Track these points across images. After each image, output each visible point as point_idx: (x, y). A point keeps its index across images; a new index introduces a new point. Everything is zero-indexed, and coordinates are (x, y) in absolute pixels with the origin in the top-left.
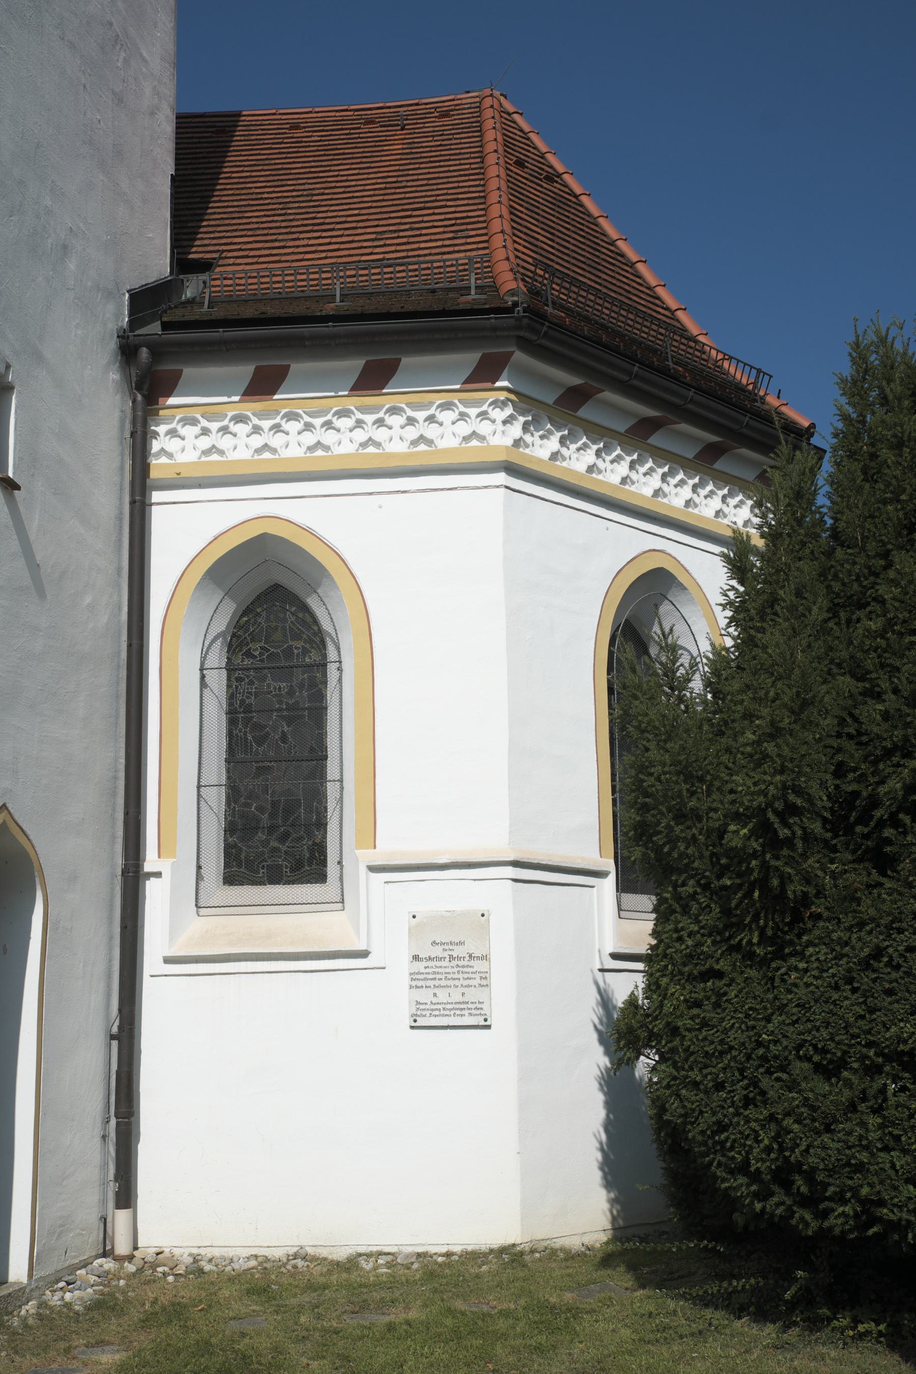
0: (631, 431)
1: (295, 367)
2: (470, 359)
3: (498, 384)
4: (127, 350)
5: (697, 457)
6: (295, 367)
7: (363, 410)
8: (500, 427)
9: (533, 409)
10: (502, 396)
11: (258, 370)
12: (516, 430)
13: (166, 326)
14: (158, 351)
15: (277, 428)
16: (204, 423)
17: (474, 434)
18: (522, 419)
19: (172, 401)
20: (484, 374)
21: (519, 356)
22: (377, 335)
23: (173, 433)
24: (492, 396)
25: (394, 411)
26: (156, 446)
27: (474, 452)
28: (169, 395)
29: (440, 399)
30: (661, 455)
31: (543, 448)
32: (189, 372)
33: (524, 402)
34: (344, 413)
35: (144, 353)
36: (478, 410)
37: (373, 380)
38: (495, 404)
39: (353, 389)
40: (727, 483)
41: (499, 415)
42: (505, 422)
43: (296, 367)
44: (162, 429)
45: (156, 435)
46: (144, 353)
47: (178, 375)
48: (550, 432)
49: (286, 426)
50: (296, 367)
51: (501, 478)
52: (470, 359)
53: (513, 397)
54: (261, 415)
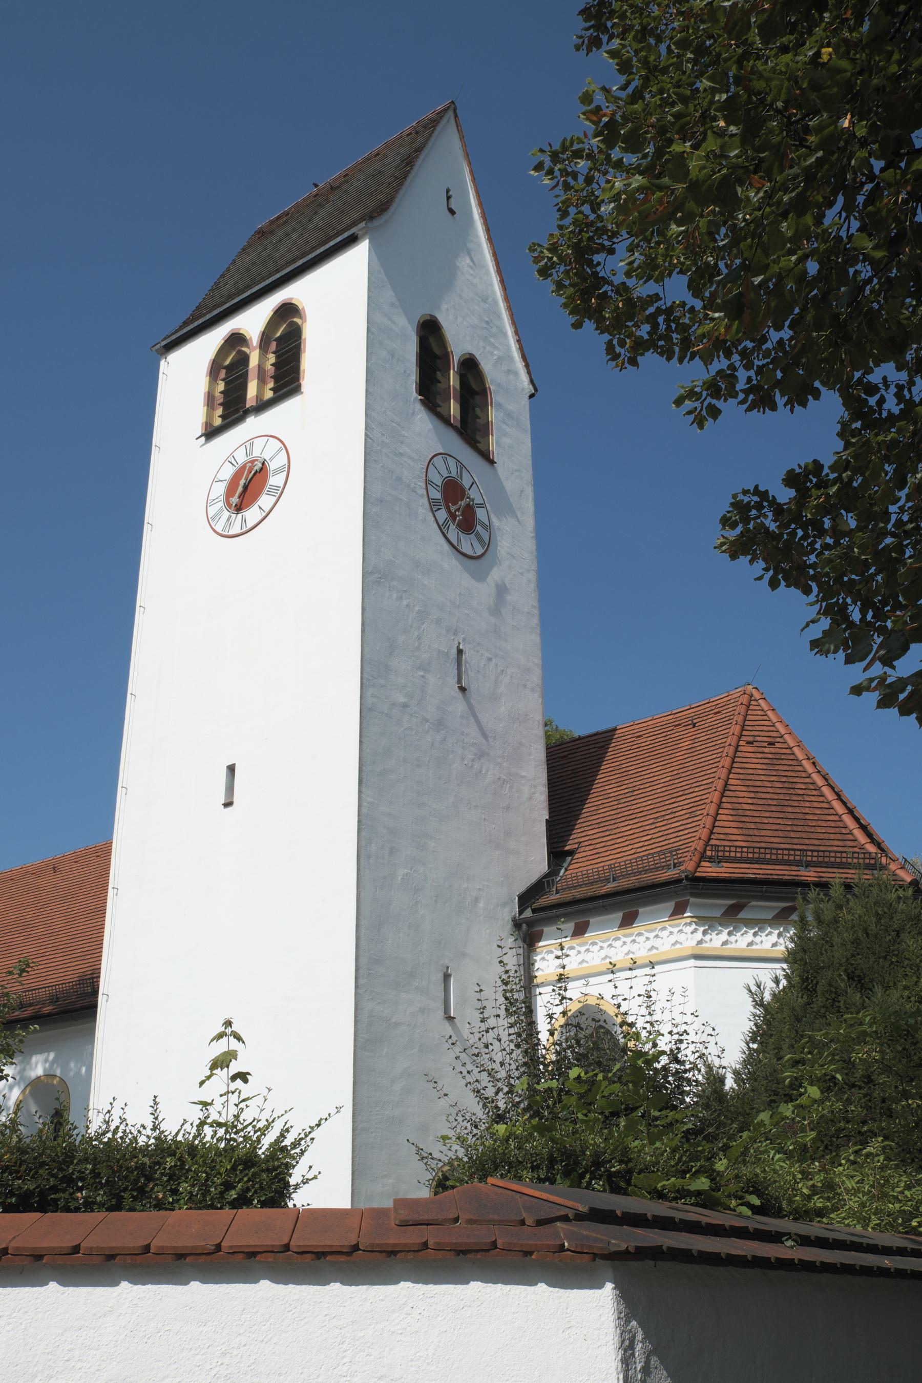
0: (725, 914)
1: (592, 920)
2: (671, 905)
3: (686, 915)
4: (517, 924)
5: (723, 915)
6: (592, 920)
7: (625, 936)
8: (690, 935)
9: (708, 922)
10: (689, 920)
11: (576, 924)
12: (699, 936)
13: (534, 911)
14: (530, 923)
15: (588, 950)
16: (600, 944)
17: (677, 942)
18: (702, 929)
19: (541, 944)
20: (678, 911)
21: (692, 900)
22: (626, 900)
23: (543, 959)
24: (683, 921)
25: (640, 934)
26: (537, 966)
27: (679, 951)
28: (539, 941)
29: (659, 926)
30: (749, 923)
31: (717, 940)
32: (546, 930)
33: (700, 920)
34: (617, 939)
35: (524, 926)
36: (678, 929)
37: (628, 921)
38: (686, 924)
39: (620, 927)
40: (756, 925)
41: (689, 929)
42: (692, 933)
43: (592, 920)
44: (538, 958)
45: (536, 961)
46: (524, 926)
47: (542, 932)
48: (722, 931)
49: (592, 948)
50: (592, 920)
51: (692, 962)
52: (671, 905)
53: (695, 920)
54: (580, 945)
